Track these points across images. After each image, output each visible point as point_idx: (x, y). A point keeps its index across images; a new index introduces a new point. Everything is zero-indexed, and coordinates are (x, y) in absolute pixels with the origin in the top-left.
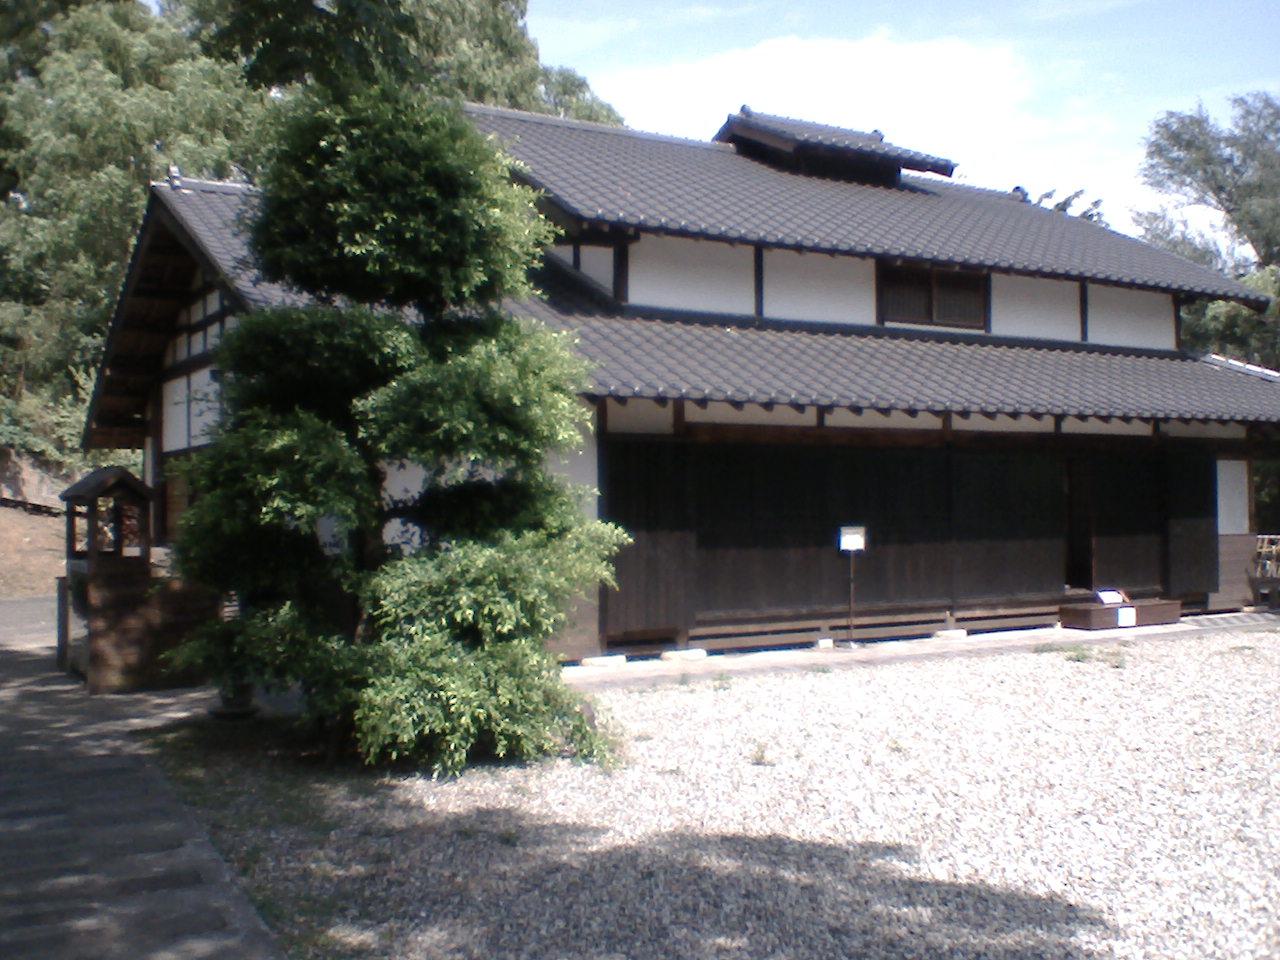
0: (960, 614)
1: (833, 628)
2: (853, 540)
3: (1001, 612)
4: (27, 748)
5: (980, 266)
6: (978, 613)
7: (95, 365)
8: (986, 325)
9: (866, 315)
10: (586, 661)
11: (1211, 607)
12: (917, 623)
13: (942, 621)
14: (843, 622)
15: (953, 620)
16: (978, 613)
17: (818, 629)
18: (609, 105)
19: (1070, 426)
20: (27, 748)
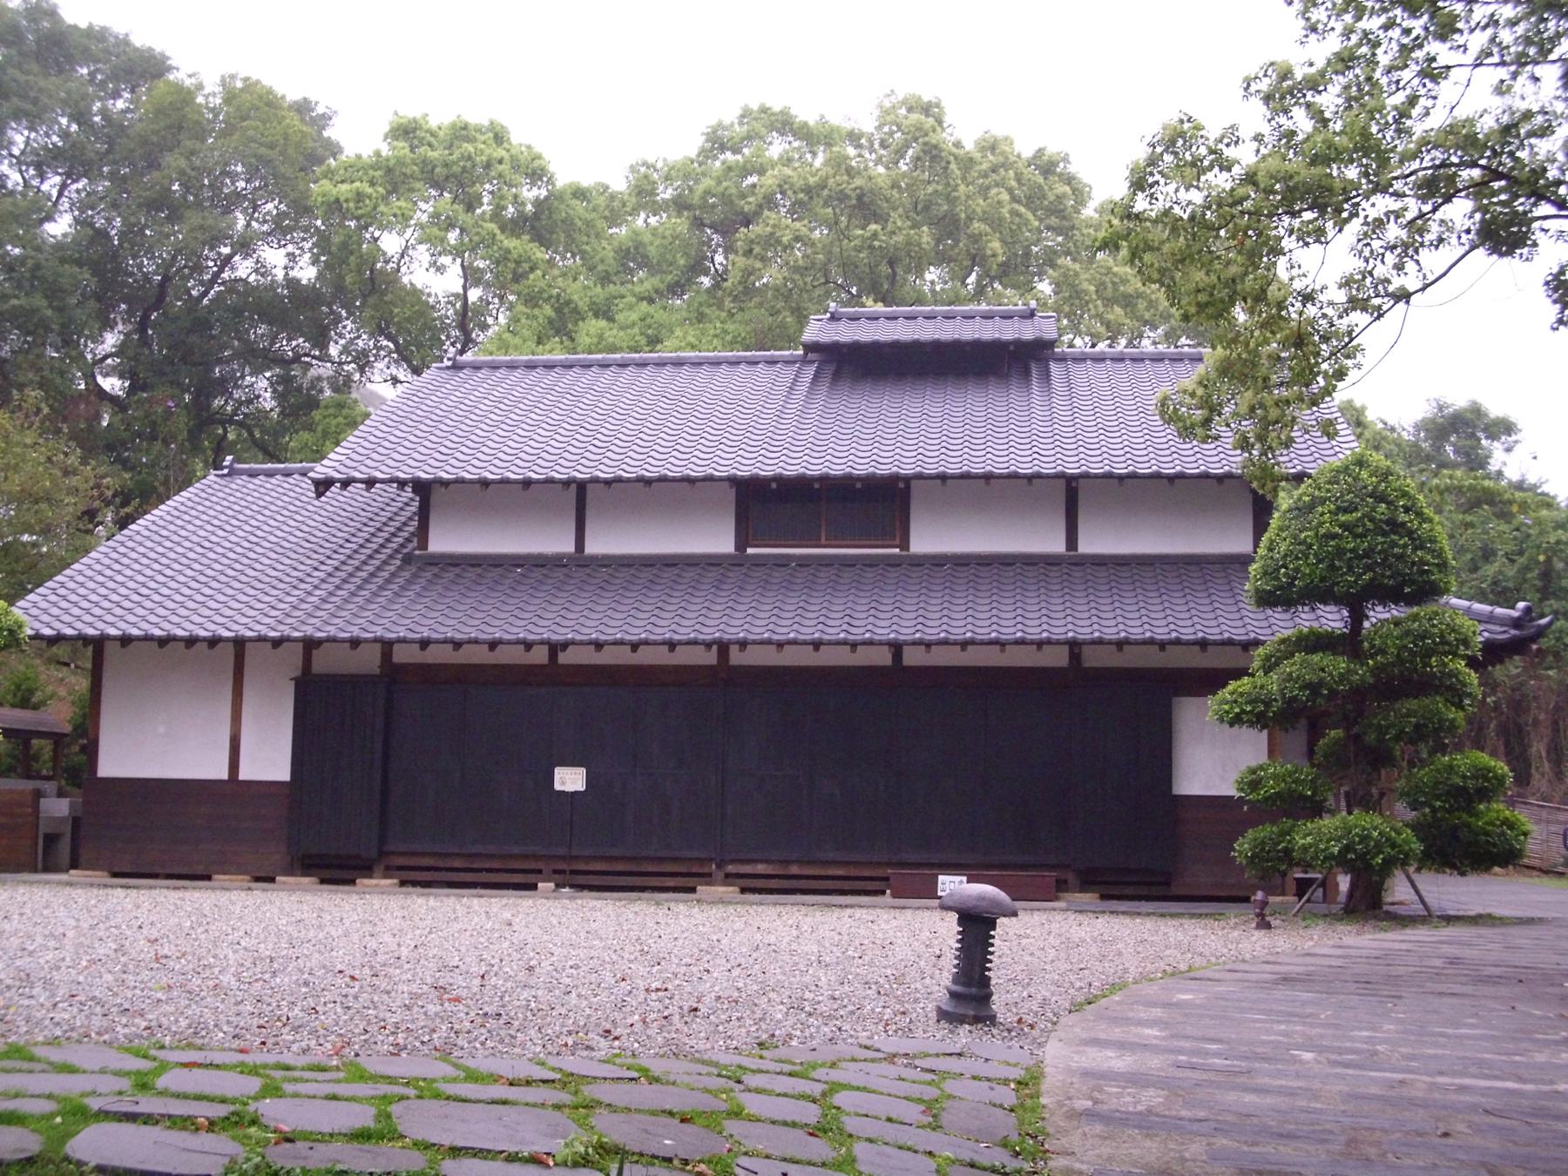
0: (731, 868)
1: (555, 872)
2: (570, 779)
3: (794, 870)
4: (1191, 997)
5: (895, 478)
6: (761, 868)
7: (1484, 214)
8: (905, 545)
9: (723, 543)
10: (216, 877)
11: (1175, 891)
12: (428, 869)
13: (710, 875)
14: (563, 866)
15: (720, 875)
16: (761, 868)
17: (540, 872)
18: (1047, 166)
19: (912, 658)
20: (1191, 997)
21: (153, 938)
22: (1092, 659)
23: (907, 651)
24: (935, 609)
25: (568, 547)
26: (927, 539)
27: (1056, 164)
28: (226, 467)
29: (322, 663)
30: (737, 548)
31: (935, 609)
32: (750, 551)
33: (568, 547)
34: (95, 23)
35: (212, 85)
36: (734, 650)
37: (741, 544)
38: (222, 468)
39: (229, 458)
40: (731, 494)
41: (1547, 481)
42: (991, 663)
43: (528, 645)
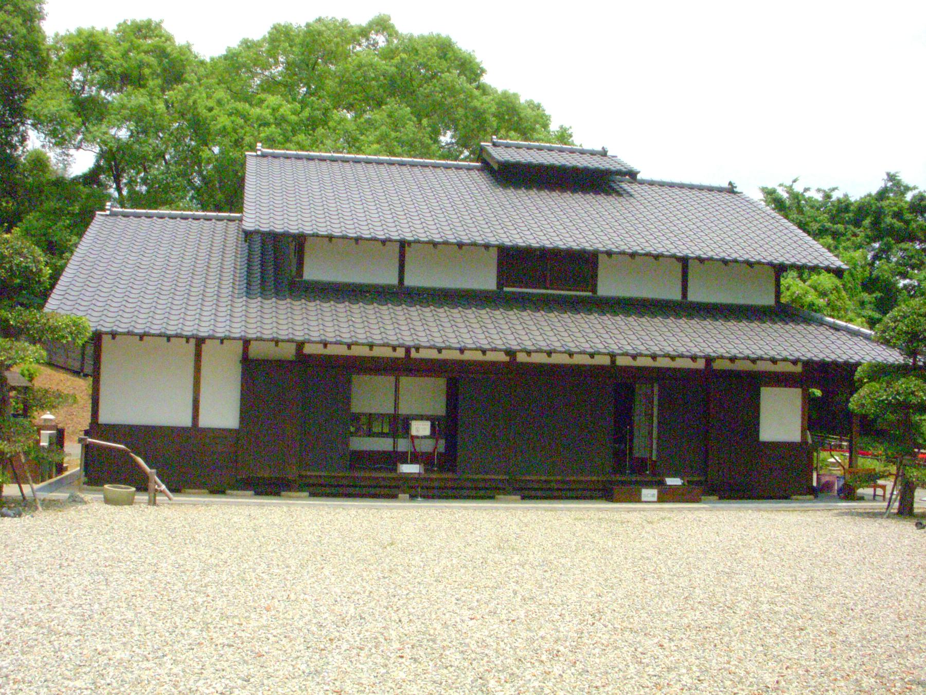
8: (594, 290)
21: (68, 636)
22: (718, 365)
23: (253, 345)
24: (168, 284)
25: (393, 280)
26: (606, 288)
27: (389, 28)
28: (108, 210)
29: (256, 351)
30: (498, 288)
31: (168, 284)
33: (393, 280)
35: (208, 60)
36: (413, 351)
37: (500, 284)
38: (104, 210)
39: (109, 204)
41: (571, 127)
42: (563, 362)
43: (694, 358)
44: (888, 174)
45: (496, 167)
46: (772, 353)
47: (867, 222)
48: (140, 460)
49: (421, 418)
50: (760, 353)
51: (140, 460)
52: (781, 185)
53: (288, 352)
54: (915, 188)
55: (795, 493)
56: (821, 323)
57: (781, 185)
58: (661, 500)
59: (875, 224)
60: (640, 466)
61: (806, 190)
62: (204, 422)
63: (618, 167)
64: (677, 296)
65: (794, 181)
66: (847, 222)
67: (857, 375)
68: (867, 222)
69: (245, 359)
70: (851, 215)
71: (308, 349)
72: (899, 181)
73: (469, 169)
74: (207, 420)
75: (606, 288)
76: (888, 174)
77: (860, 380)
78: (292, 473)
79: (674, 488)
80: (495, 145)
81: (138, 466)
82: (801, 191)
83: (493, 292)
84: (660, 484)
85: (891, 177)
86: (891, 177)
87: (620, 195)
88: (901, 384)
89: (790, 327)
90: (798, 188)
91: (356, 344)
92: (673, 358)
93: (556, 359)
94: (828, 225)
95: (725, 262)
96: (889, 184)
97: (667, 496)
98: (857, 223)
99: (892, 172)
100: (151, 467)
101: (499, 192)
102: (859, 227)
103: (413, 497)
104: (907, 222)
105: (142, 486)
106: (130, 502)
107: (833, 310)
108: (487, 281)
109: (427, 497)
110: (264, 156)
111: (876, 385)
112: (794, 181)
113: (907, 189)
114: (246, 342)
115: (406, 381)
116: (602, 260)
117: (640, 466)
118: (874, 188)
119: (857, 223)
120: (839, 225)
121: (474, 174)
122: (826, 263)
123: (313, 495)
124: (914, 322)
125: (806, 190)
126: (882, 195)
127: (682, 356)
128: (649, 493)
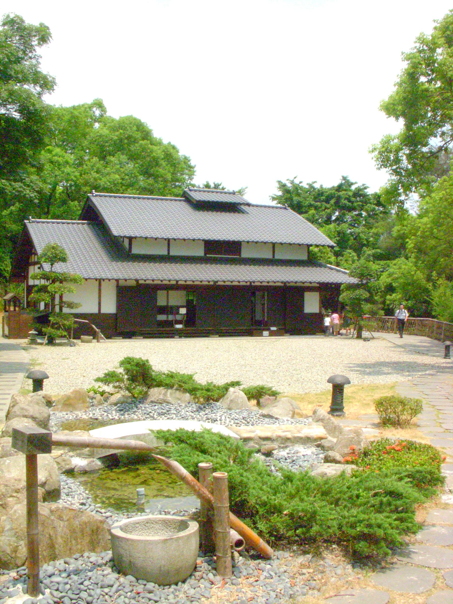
8: (240, 254)
23: (120, 281)
25: (165, 253)
26: (245, 254)
29: (122, 283)
32: (208, 256)
34: (352, 179)
37: (205, 254)
40: (203, 243)
44: (343, 177)
45: (195, 202)
46: (310, 280)
47: (332, 202)
48: (94, 326)
49: (183, 307)
50: (305, 280)
51: (94, 326)
52: (288, 180)
53: (133, 283)
54: (356, 183)
55: (317, 332)
56: (326, 267)
57: (288, 180)
58: (270, 335)
59: (337, 203)
60: (259, 323)
61: (301, 183)
62: (103, 311)
63: (243, 202)
64: (271, 257)
65: (295, 178)
66: (323, 201)
67: (341, 288)
68: (332, 202)
69: (118, 286)
70: (324, 197)
71: (141, 282)
72: (348, 181)
73: (180, 201)
74: (104, 310)
75: (245, 254)
76: (343, 177)
77: (342, 290)
78: (138, 329)
79: (273, 331)
80: (191, 190)
81: (93, 329)
82: (298, 183)
83: (202, 257)
84: (269, 329)
85: (344, 178)
86: (344, 178)
87: (243, 213)
88: (358, 292)
89: (314, 268)
90: (297, 181)
91: (148, 279)
92: (275, 283)
93: (234, 284)
94: (313, 203)
95: (290, 244)
96: (343, 182)
97: (272, 334)
98: (327, 201)
99: (345, 176)
100: (98, 328)
101: (197, 213)
102: (328, 203)
103: (180, 337)
104: (352, 202)
105: (95, 335)
106: (90, 342)
107: (321, 253)
108: (200, 252)
109: (186, 337)
110: (96, 196)
111: (349, 292)
112: (295, 178)
113: (352, 184)
114: (117, 281)
115: (171, 293)
116: (242, 243)
117: (259, 323)
118: (336, 182)
119: (327, 201)
120: (318, 203)
121: (183, 203)
122: (328, 244)
123: (144, 338)
124: (362, 270)
125: (301, 183)
126: (339, 188)
127: (278, 282)
128: (266, 333)
